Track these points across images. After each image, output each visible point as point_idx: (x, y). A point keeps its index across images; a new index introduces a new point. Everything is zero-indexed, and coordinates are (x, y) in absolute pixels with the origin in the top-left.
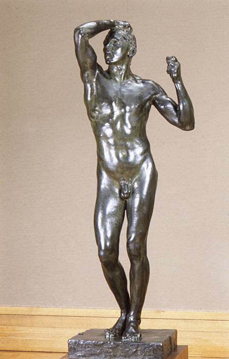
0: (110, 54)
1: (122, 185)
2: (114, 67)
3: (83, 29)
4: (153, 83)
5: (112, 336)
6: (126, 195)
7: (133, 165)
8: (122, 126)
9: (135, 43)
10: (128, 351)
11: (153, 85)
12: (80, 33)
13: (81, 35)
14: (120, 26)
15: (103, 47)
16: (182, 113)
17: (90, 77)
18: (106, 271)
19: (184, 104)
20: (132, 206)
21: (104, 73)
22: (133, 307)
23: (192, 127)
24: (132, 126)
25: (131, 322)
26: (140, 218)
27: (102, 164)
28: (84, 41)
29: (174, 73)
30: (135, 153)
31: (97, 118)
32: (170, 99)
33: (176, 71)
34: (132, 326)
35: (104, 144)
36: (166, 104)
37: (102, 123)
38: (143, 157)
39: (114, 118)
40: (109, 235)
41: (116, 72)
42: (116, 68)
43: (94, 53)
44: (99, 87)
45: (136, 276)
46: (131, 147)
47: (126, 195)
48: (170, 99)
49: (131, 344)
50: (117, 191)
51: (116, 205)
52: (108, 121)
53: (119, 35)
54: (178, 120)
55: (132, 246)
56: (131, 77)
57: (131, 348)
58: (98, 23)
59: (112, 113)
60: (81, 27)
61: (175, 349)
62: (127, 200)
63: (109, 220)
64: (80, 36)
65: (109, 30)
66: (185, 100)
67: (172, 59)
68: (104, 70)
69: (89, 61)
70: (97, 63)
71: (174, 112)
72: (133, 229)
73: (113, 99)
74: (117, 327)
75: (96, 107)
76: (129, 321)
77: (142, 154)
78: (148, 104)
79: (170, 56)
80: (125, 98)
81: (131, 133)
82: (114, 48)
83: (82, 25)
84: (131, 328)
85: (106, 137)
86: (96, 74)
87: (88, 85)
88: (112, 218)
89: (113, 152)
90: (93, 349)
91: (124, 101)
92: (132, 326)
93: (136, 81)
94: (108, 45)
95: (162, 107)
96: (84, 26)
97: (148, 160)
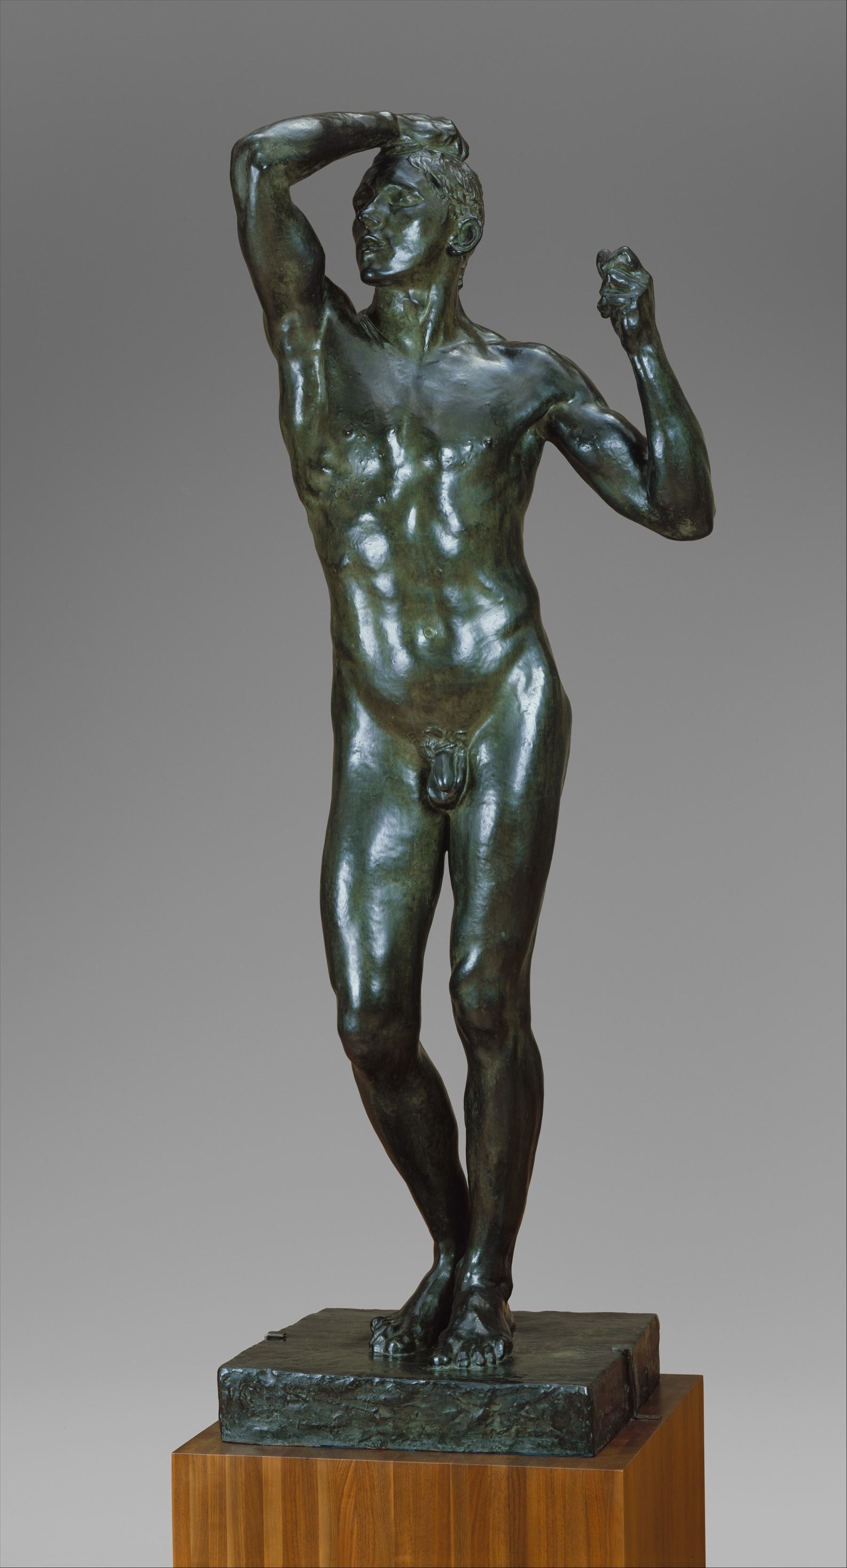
0: (377, 243)
1: (429, 753)
2: (393, 296)
3: (267, 146)
4: (550, 359)
5: (396, 1350)
6: (443, 795)
7: (471, 675)
8: (422, 522)
9: (479, 201)
10: (453, 1417)
11: (546, 363)
12: (252, 161)
13: (259, 167)
14: (419, 136)
15: (351, 215)
16: (663, 472)
17: (300, 335)
18: (372, 1092)
19: (671, 433)
20: (468, 836)
21: (357, 319)
22: (481, 1230)
23: (704, 527)
24: (462, 521)
25: (472, 1290)
26: (498, 885)
27: (353, 672)
28: (269, 192)
29: (628, 315)
30: (478, 630)
31: (329, 495)
32: (616, 415)
33: (634, 306)
34: (477, 1310)
35: (359, 599)
36: (600, 438)
37: (347, 511)
38: (508, 644)
39: (396, 493)
40: (379, 949)
41: (405, 315)
42: (401, 295)
43: (311, 238)
44: (334, 372)
45: (491, 1109)
46: (464, 606)
47: (443, 795)
48: (616, 415)
49: (466, 1386)
50: (411, 778)
51: (406, 832)
52: (370, 507)
53: (416, 168)
54: (648, 498)
55: (469, 992)
56: (461, 332)
57: (463, 1403)
58: (327, 124)
59: (388, 470)
60: (260, 135)
61: (645, 1399)
62: (450, 813)
63: (378, 893)
64: (255, 172)
65: (377, 150)
66: (673, 420)
67: (621, 259)
68: (358, 310)
69: (292, 270)
70: (327, 280)
71: (630, 466)
72: (474, 926)
73: (390, 419)
74: (417, 1313)
75: (322, 450)
76: (464, 1288)
77: (505, 633)
78: (529, 438)
79: (611, 248)
80: (438, 412)
81: (463, 552)
82: (393, 220)
83: (261, 130)
84: (472, 1316)
85: (365, 569)
86: (325, 322)
87: (295, 367)
88: (392, 885)
89: (392, 628)
90: (317, 1407)
91: (436, 428)
92: (477, 1310)
93: (482, 348)
94: (370, 208)
95: (585, 448)
96: (270, 133)
97: (531, 655)
